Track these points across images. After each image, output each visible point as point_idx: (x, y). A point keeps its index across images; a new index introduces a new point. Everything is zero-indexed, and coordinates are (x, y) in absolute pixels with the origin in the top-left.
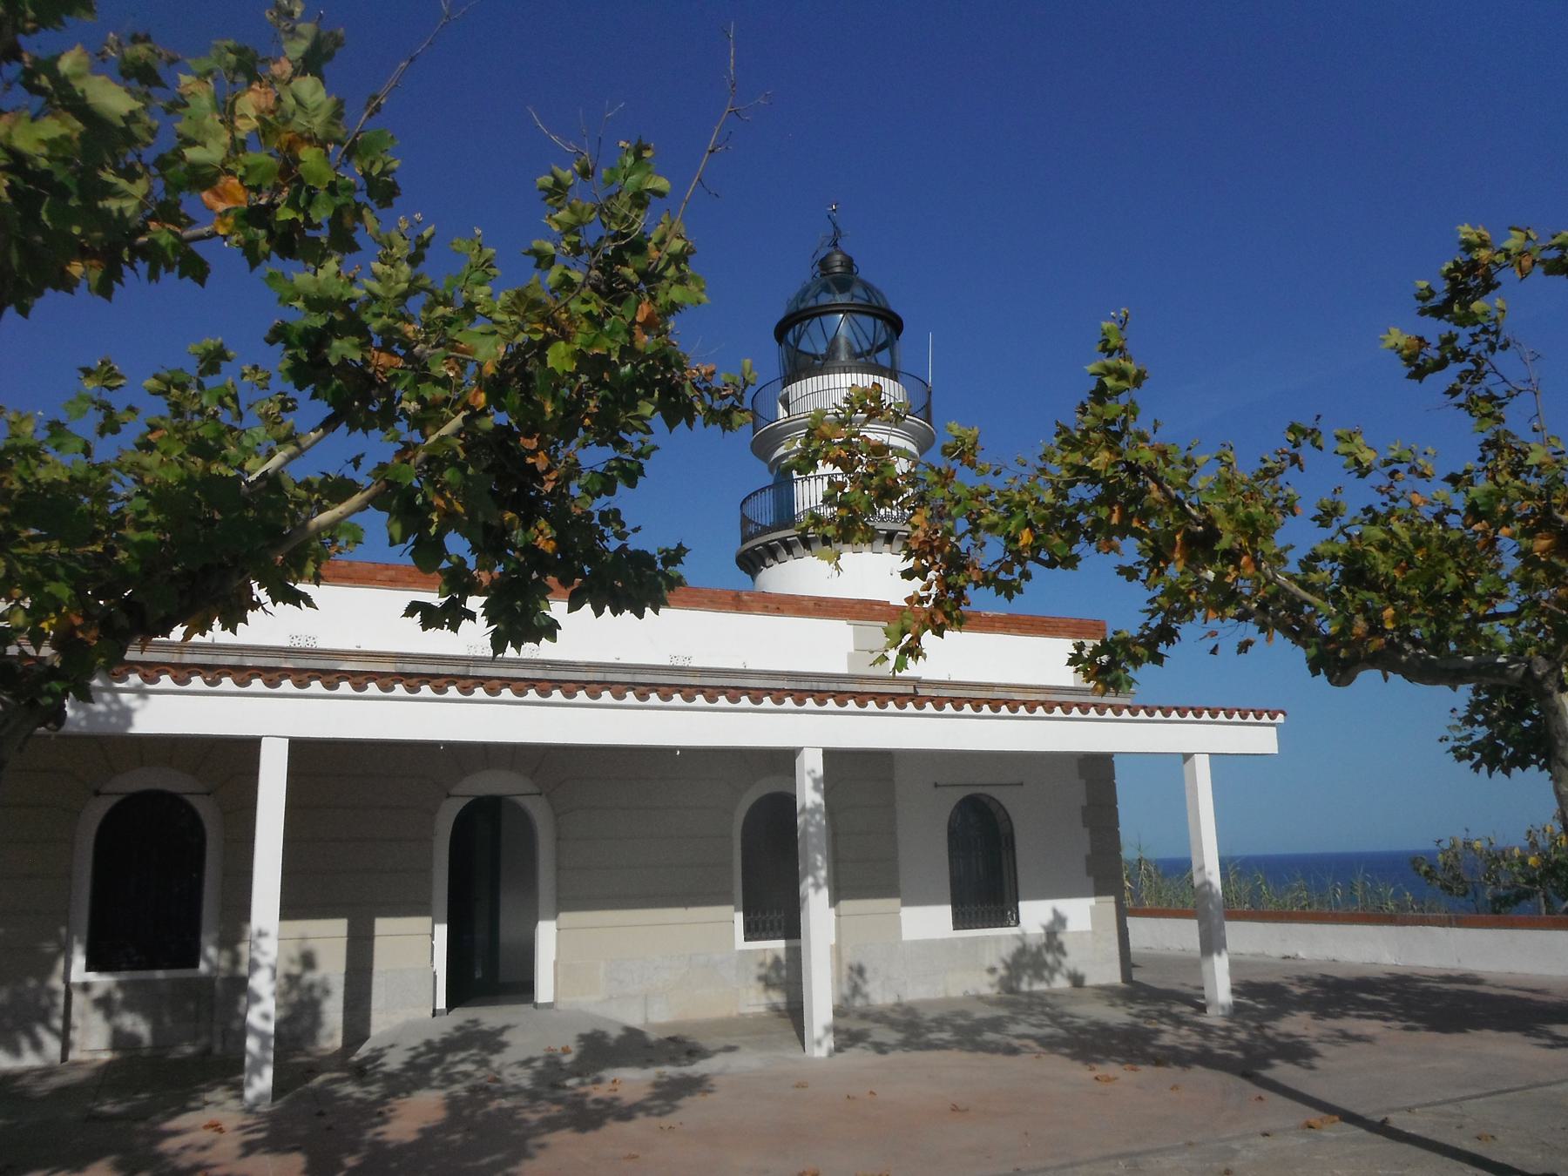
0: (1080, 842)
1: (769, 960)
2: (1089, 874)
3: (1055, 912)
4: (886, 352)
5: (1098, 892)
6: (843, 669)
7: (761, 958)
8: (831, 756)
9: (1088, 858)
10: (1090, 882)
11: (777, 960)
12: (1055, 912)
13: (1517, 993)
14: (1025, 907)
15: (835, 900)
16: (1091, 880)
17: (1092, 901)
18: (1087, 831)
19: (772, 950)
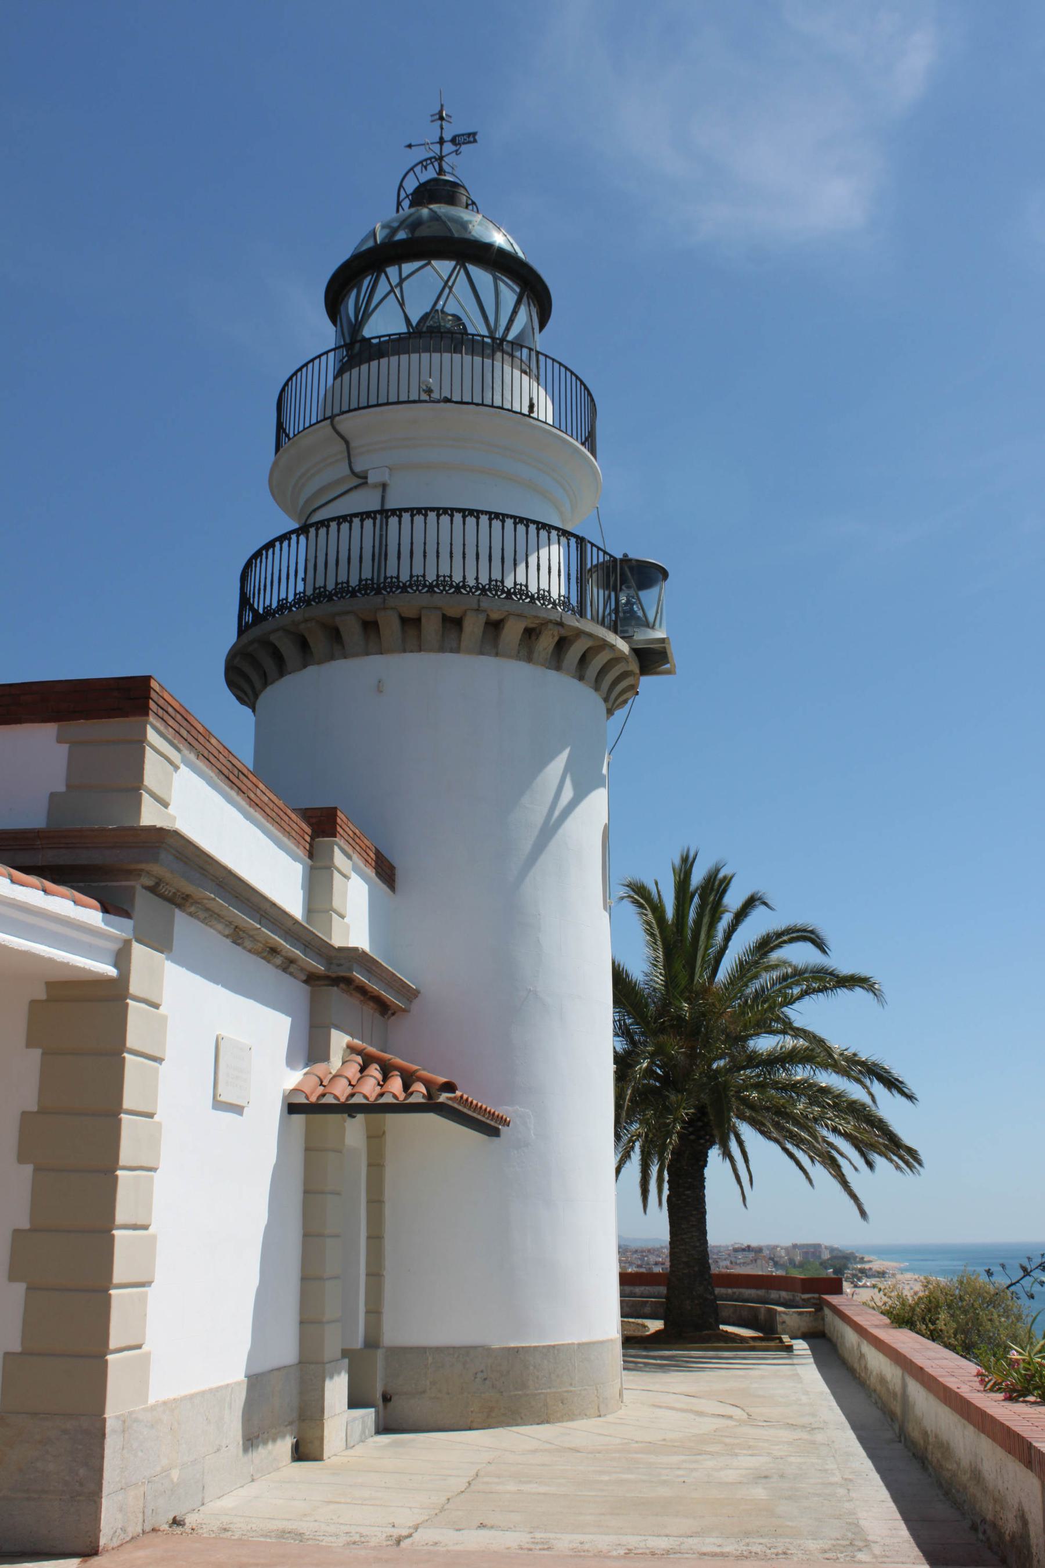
18: (36, 1054)
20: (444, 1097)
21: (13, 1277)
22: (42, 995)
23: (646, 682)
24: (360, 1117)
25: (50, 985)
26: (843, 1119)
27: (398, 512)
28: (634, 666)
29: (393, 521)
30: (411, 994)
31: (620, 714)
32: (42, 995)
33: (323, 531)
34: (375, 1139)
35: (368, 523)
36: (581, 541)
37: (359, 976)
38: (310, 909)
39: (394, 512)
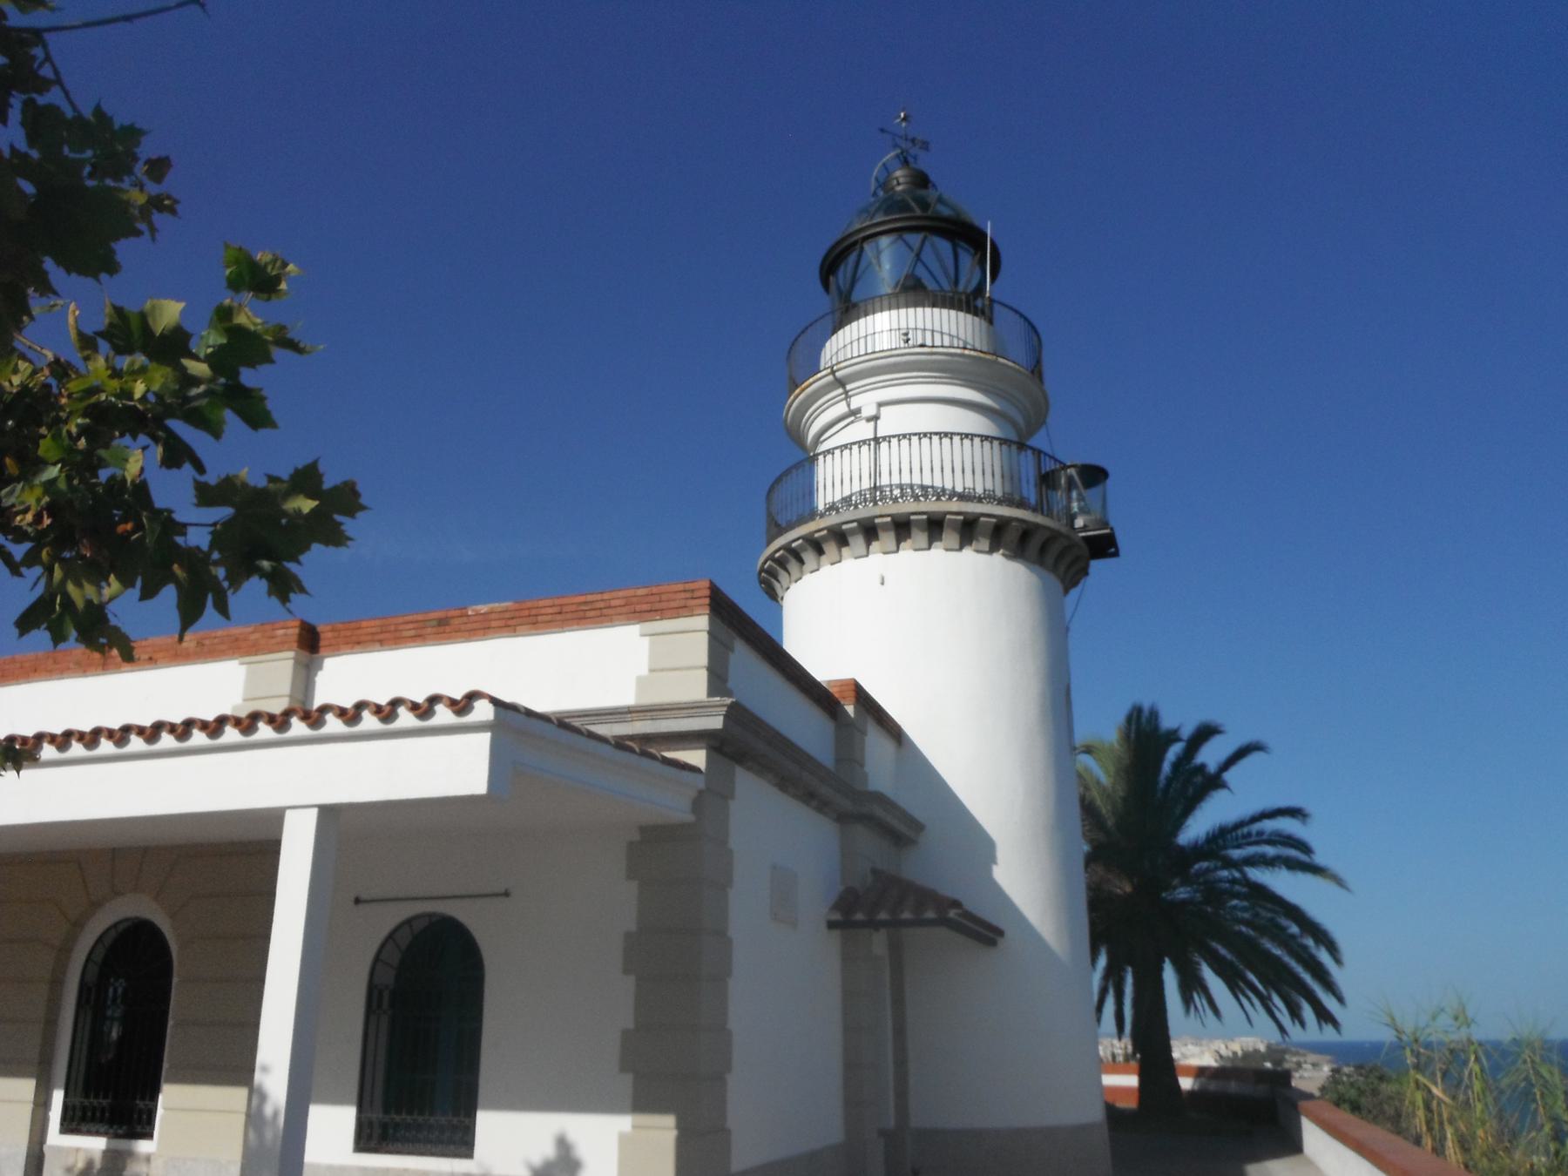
0: (615, 1003)
1: (80, 1165)
2: (624, 1068)
3: (563, 1144)
4: (47, 65)
5: (641, 1104)
6: (628, 698)
7: (70, 1161)
8: (330, 816)
9: (626, 1034)
10: (625, 1084)
11: (90, 1164)
12: (563, 1144)
13: (380, 1076)
14: (489, 1124)
15: (370, 1138)
16: (628, 1079)
17: (623, 1123)
18: (631, 980)
19: (86, 1150)
20: (952, 914)
21: (626, 971)
22: (637, 837)
23: (1096, 566)
24: (883, 931)
25: (643, 830)
26: (1281, 959)
27: (888, 439)
28: (1085, 550)
29: (884, 445)
30: (918, 827)
31: (1074, 592)
32: (637, 837)
33: (829, 457)
34: (896, 949)
35: (865, 448)
36: (1040, 452)
37: (879, 812)
38: (838, 761)
39: (884, 438)
